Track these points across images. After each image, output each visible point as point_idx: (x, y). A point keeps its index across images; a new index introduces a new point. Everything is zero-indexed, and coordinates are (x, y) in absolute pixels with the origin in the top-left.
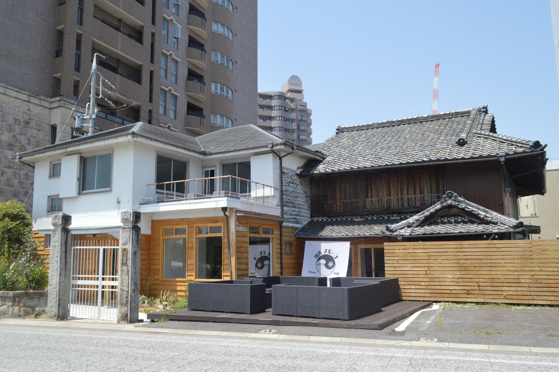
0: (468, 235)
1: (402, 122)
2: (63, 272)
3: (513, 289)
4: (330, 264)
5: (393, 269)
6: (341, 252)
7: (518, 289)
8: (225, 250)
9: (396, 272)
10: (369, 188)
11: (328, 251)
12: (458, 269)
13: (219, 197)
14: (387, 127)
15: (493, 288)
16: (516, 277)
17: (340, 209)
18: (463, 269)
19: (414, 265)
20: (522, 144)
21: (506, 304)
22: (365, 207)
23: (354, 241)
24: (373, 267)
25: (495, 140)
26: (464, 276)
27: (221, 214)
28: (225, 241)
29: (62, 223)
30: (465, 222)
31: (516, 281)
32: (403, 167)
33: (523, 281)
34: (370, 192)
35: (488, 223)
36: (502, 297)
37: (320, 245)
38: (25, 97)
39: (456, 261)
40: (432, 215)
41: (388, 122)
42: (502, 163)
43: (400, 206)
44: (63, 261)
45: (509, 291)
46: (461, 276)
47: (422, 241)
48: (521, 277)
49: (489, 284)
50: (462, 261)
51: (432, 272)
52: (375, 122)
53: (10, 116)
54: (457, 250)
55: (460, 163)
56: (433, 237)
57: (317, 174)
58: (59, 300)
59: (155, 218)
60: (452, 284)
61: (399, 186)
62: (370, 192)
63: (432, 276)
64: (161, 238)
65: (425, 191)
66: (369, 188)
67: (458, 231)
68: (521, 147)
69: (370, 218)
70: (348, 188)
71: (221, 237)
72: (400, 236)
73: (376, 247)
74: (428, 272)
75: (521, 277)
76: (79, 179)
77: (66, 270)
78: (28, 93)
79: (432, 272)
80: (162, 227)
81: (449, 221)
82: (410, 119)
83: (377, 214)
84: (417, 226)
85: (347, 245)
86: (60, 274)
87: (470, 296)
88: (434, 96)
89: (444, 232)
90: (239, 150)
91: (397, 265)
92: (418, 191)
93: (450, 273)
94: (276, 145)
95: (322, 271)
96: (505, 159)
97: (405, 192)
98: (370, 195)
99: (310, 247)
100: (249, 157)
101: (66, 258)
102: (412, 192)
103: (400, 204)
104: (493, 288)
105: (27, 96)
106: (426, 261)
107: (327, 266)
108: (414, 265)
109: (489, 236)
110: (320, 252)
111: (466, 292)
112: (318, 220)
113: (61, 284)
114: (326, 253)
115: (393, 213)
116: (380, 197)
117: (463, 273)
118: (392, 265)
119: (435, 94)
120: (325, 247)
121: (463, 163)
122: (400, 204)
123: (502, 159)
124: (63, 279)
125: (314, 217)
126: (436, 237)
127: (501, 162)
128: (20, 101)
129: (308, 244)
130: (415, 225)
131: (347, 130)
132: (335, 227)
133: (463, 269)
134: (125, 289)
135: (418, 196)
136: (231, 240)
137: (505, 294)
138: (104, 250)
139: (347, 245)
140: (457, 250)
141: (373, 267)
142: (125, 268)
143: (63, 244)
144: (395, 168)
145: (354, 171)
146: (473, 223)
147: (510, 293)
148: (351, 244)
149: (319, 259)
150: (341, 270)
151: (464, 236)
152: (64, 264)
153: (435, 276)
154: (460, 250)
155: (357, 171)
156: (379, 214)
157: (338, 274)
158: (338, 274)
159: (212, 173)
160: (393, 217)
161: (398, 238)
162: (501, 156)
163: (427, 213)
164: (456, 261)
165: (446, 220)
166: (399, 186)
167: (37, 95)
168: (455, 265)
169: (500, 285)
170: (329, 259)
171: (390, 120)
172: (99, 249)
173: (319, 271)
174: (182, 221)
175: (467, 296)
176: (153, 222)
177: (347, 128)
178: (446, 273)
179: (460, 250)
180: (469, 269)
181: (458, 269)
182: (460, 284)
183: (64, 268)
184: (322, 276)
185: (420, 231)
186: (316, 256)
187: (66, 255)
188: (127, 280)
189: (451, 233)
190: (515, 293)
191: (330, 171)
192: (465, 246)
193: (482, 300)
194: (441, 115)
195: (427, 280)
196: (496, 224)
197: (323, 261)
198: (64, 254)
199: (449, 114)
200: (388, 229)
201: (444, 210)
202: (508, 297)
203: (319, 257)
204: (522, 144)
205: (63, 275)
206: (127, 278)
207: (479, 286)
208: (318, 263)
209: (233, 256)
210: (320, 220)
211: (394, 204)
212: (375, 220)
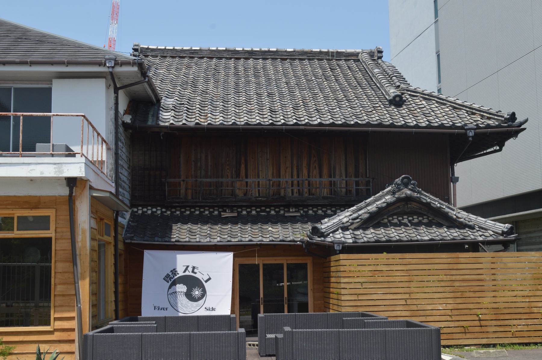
0: (442, 244)
1: (251, 54)
3: (523, 322)
4: (197, 293)
5: (355, 297)
6: (218, 272)
7: (530, 322)
8: (58, 267)
9: (359, 303)
10: (243, 161)
11: (190, 269)
12: (452, 295)
13: (53, 155)
14: (227, 58)
15: (499, 323)
16: (526, 305)
17: (186, 194)
18: (459, 295)
19: (388, 290)
20: (490, 114)
21: (519, 344)
22: (233, 194)
23: (239, 250)
24: (262, 295)
25: (444, 104)
26: (461, 306)
27: (65, 191)
28: (59, 248)
30: (429, 225)
32: (325, 131)
34: (243, 166)
35: (462, 226)
36: (510, 335)
37: (175, 259)
39: (449, 284)
40: (381, 211)
41: (227, 51)
45: (520, 325)
46: (456, 306)
47: (388, 252)
48: (533, 304)
49: (494, 317)
50: (457, 284)
51: (415, 302)
52: (205, 47)
54: (451, 266)
55: (411, 133)
56: (390, 246)
57: (166, 127)
60: (443, 318)
62: (243, 166)
63: (414, 308)
65: (337, 172)
66: (243, 161)
67: (236, 240)
68: (489, 118)
69: (178, 213)
71: (50, 239)
72: (339, 243)
73: (289, 262)
74: (409, 302)
75: (533, 304)
79: (415, 302)
81: (389, 221)
82: (265, 52)
83: (257, 207)
84: (356, 229)
85: (229, 257)
87: (468, 336)
88: (113, 14)
89: (373, 240)
90: (32, 63)
91: (361, 291)
92: (325, 171)
93: (441, 301)
94: (123, 64)
95: (179, 305)
96: (475, 134)
97: (305, 172)
98: (243, 173)
99: (153, 262)
100: (50, 78)
102: (316, 172)
104: (499, 323)
106: (406, 284)
107: (189, 296)
108: (388, 290)
109: (475, 246)
110: (174, 272)
111: (462, 330)
112: (143, 212)
114: (187, 273)
115: (287, 206)
116: (260, 178)
117: (459, 300)
118: (353, 291)
119: (115, 13)
120: (184, 261)
121: (416, 133)
123: (471, 134)
125: (137, 206)
126: (395, 246)
127: (469, 137)
129: (150, 258)
130: (353, 227)
131: (153, 54)
132: (248, 227)
133: (459, 295)
135: (325, 180)
136: (79, 245)
137: (514, 329)
139: (229, 257)
140: (451, 266)
141: (262, 295)
144: (288, 131)
145: (238, 129)
146: (440, 226)
147: (519, 328)
148: (234, 256)
149: (174, 284)
150: (219, 300)
151: (437, 245)
153: (420, 307)
154: (455, 266)
155: (244, 129)
156: (260, 207)
157: (213, 309)
158: (213, 309)
160: (289, 211)
161: (336, 247)
162: (470, 129)
163: (372, 208)
164: (449, 284)
165: (395, 221)
166: (295, 162)
168: (448, 289)
169: (507, 317)
170: (194, 285)
171: (231, 47)
173: (174, 307)
175: (463, 336)
177: (153, 50)
178: (435, 301)
179: (455, 266)
180: (467, 295)
181: (452, 295)
182: (454, 318)
184: (181, 315)
185: (370, 235)
186: (167, 278)
189: (417, 241)
190: (525, 328)
191: (192, 124)
192: (462, 260)
193: (484, 341)
194: (315, 53)
195: (407, 313)
196: (472, 228)
197: (181, 288)
199: (327, 53)
200: (316, 231)
201: (398, 205)
202: (518, 334)
203: (172, 279)
204: (490, 114)
207: (480, 320)
208: (171, 291)
209: (83, 278)
211: (289, 192)
212: (253, 216)
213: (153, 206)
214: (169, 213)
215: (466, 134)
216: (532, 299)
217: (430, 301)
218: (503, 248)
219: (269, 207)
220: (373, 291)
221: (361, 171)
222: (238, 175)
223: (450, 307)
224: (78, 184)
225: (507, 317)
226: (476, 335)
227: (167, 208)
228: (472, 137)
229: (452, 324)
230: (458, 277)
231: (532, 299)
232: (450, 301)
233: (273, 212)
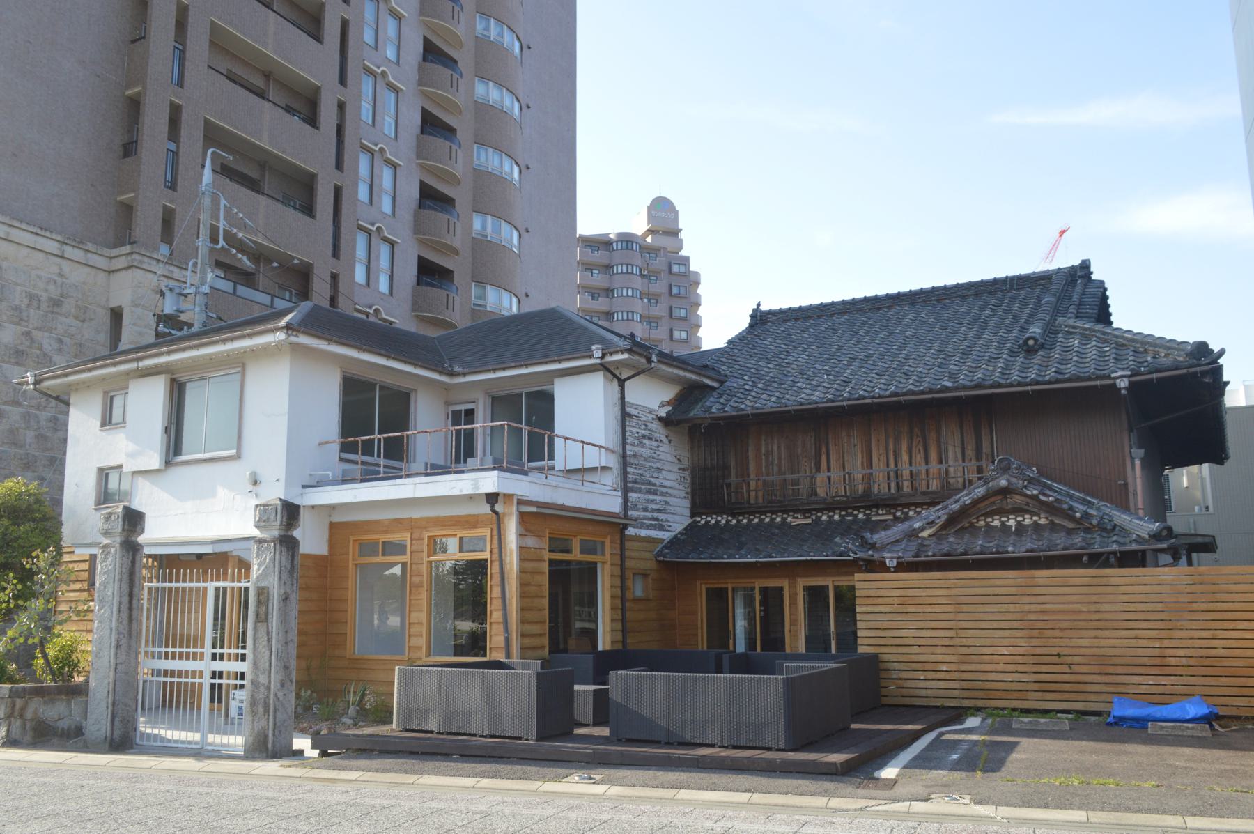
2: (124, 642)
3: (1151, 680)
7: (1163, 680)
10: (824, 450)
16: (1157, 652)
18: (1035, 633)
26: (1038, 651)
27: (485, 509)
28: (492, 569)
29: (123, 530)
31: (1157, 661)
33: (1173, 661)
38: (52, 247)
39: (1018, 616)
42: (1123, 392)
43: (893, 491)
44: (125, 615)
53: (19, 288)
54: (1021, 590)
58: (114, 704)
59: (337, 518)
61: (891, 446)
62: (824, 458)
64: (351, 562)
65: (951, 454)
66: (824, 450)
69: (824, 518)
70: (775, 448)
71: (486, 560)
76: (167, 430)
77: (130, 635)
78: (59, 238)
80: (352, 538)
83: (842, 509)
86: (118, 647)
92: (933, 455)
93: (1006, 642)
97: (905, 458)
101: (130, 609)
102: (919, 458)
103: (893, 485)
105: (56, 245)
112: (707, 522)
113: (119, 667)
117: (1035, 642)
122: (893, 485)
124: (122, 657)
125: (700, 515)
128: (41, 255)
133: (1035, 633)
134: (263, 679)
135: (934, 467)
138: (217, 589)
142: (262, 628)
143: (125, 577)
152: (126, 622)
159: (470, 415)
164: (1018, 616)
166: (891, 446)
167: (81, 242)
168: (1016, 624)
169: (1120, 670)
172: (205, 589)
174: (398, 524)
176: (332, 526)
180: (1049, 633)
183: (126, 632)
187: (130, 602)
188: (266, 658)
192: (1041, 581)
198: (126, 599)
201: (992, 499)
205: (124, 647)
206: (267, 653)
210: (713, 522)
211: (881, 487)
213: (718, 514)
214: (735, 521)
215: (1114, 384)
216: (1166, 643)
217: (988, 642)
218: (1171, 560)
219: (857, 508)
220: (901, 625)
221: (985, 450)
222: (818, 469)
223: (1021, 651)
224: (500, 498)
225: (1120, 670)
226: (1066, 696)
227: (733, 515)
228: (1126, 388)
229: (1024, 677)
230: (1033, 608)
231: (1166, 643)
232: (1022, 642)
233: (861, 516)
